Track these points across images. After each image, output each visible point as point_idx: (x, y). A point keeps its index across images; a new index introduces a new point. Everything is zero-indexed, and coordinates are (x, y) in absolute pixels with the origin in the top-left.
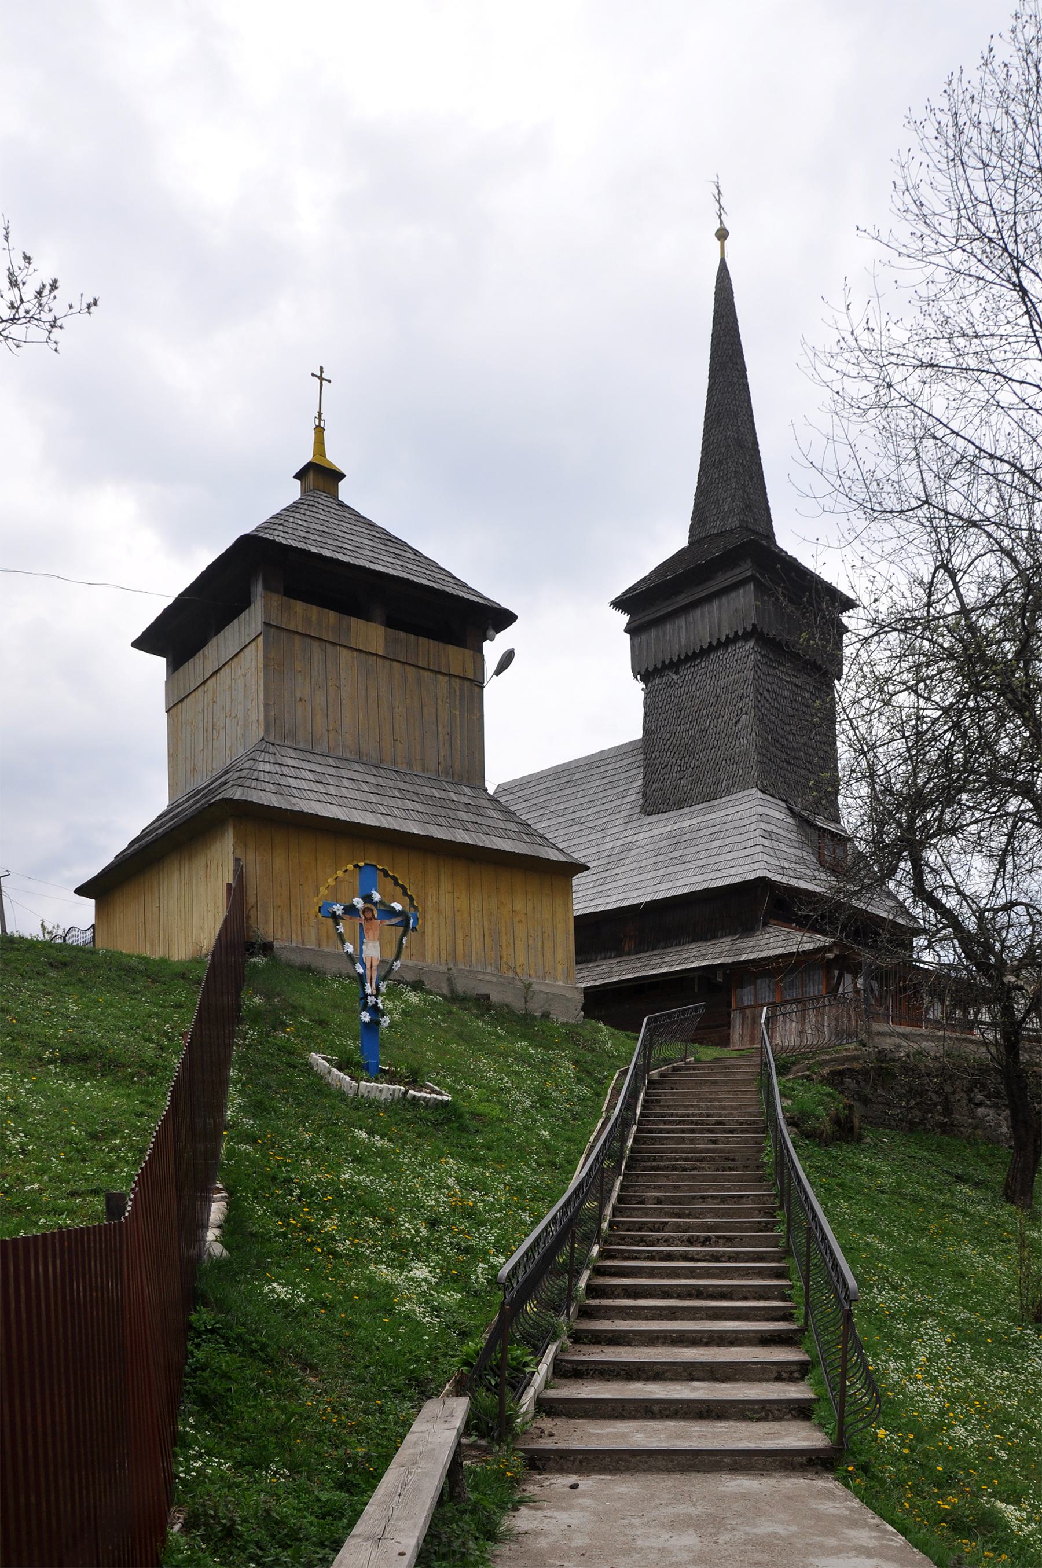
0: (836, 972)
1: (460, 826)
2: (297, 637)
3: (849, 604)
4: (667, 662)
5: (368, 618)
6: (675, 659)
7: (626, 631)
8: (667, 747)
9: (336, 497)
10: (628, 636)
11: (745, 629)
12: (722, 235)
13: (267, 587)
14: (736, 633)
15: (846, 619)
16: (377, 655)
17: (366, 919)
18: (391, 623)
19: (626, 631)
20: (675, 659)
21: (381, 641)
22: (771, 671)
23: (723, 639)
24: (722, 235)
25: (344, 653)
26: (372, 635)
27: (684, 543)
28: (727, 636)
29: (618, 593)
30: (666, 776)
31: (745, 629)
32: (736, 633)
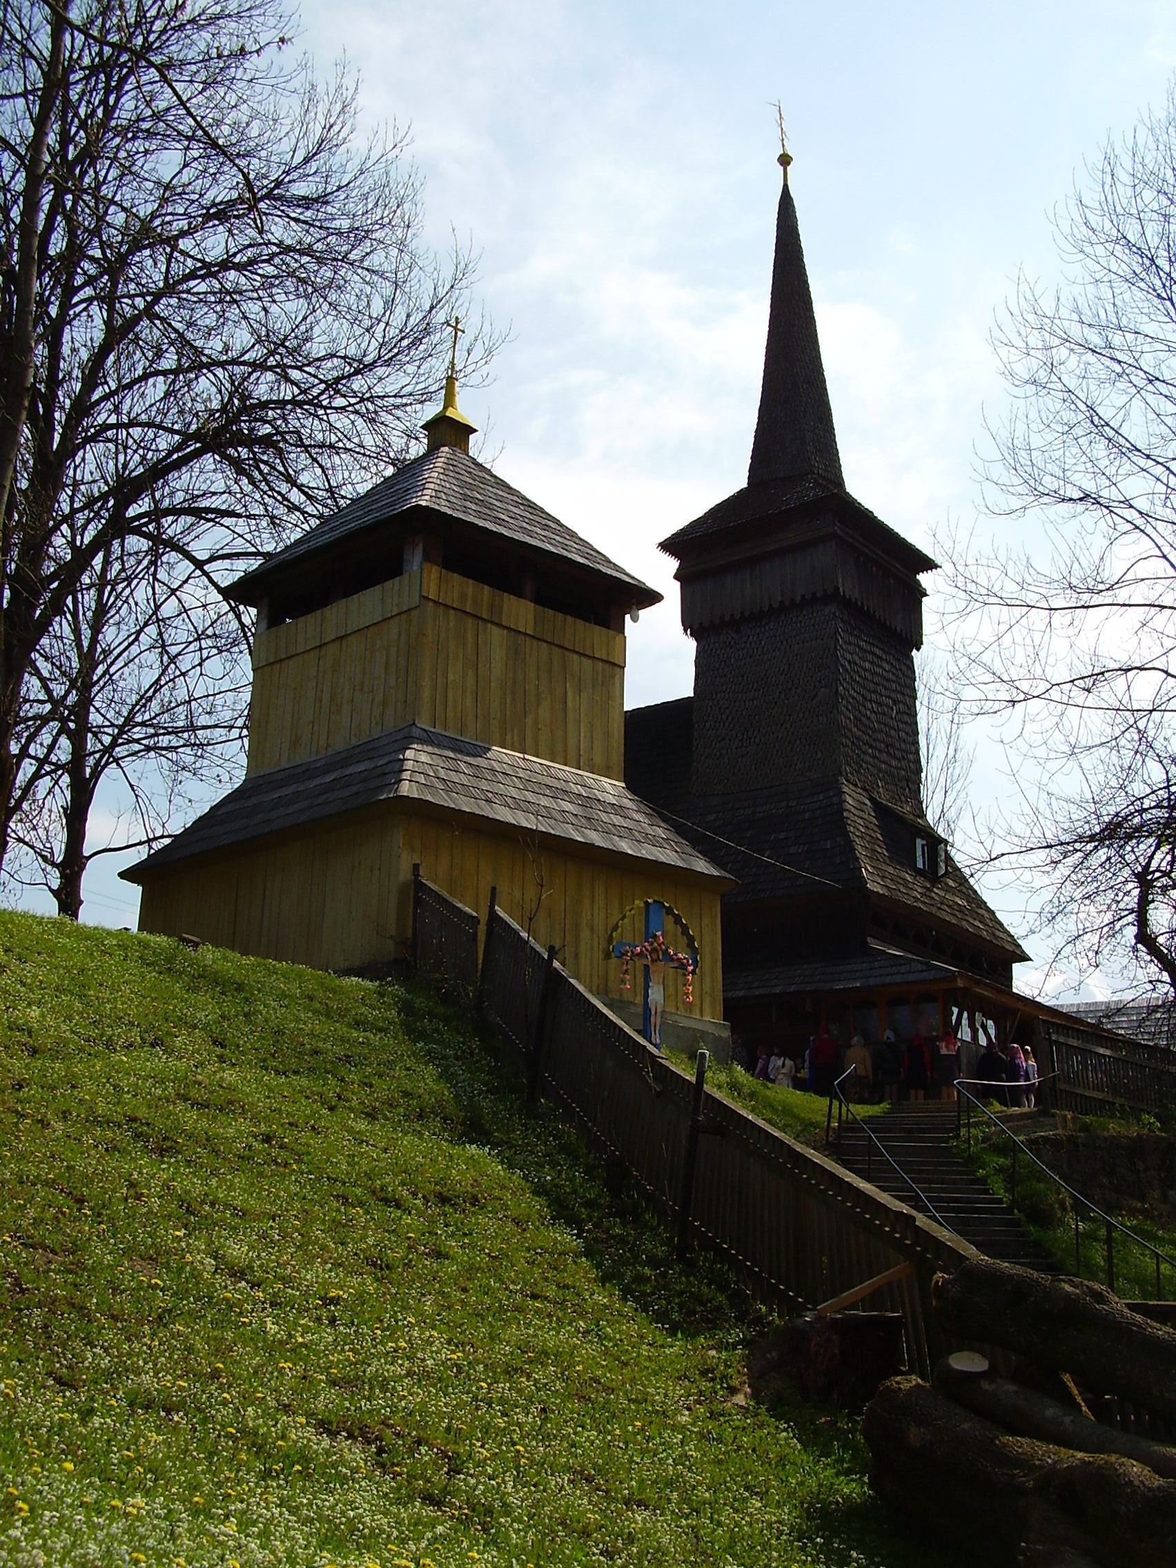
0: (955, 1010)
1: (522, 804)
2: (452, 611)
3: (928, 564)
4: (727, 618)
5: (519, 594)
6: (738, 616)
7: (676, 577)
8: (724, 717)
9: (466, 451)
10: (678, 584)
11: (825, 591)
12: (785, 160)
13: (427, 558)
14: (814, 594)
15: (924, 579)
16: (526, 634)
17: (653, 961)
18: (541, 600)
19: (676, 577)
20: (738, 616)
21: (531, 617)
22: (852, 639)
23: (798, 599)
24: (785, 160)
25: (496, 631)
26: (521, 612)
27: (739, 481)
28: (803, 596)
29: (667, 534)
30: (724, 752)
31: (825, 591)
32: (814, 594)
